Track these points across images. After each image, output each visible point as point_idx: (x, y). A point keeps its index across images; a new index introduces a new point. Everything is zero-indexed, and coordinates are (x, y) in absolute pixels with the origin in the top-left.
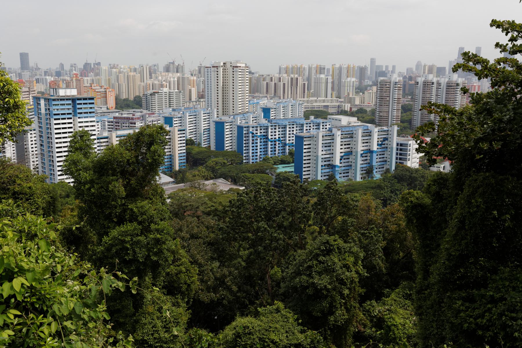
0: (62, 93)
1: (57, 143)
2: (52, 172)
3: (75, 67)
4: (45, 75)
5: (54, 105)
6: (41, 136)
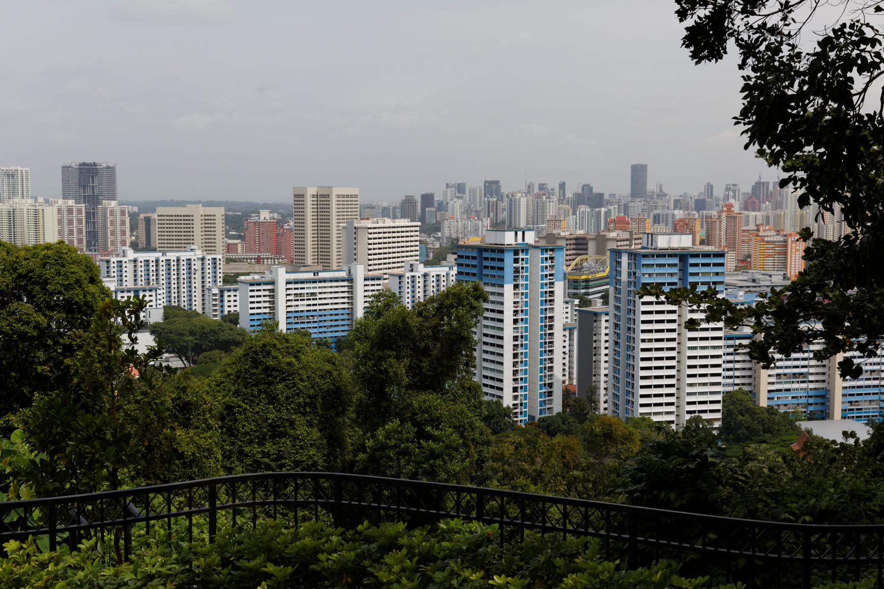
0: (662, 242)
1: (643, 341)
2: (630, 398)
3: (734, 191)
4: (675, 208)
5: (643, 265)
6: (617, 326)
